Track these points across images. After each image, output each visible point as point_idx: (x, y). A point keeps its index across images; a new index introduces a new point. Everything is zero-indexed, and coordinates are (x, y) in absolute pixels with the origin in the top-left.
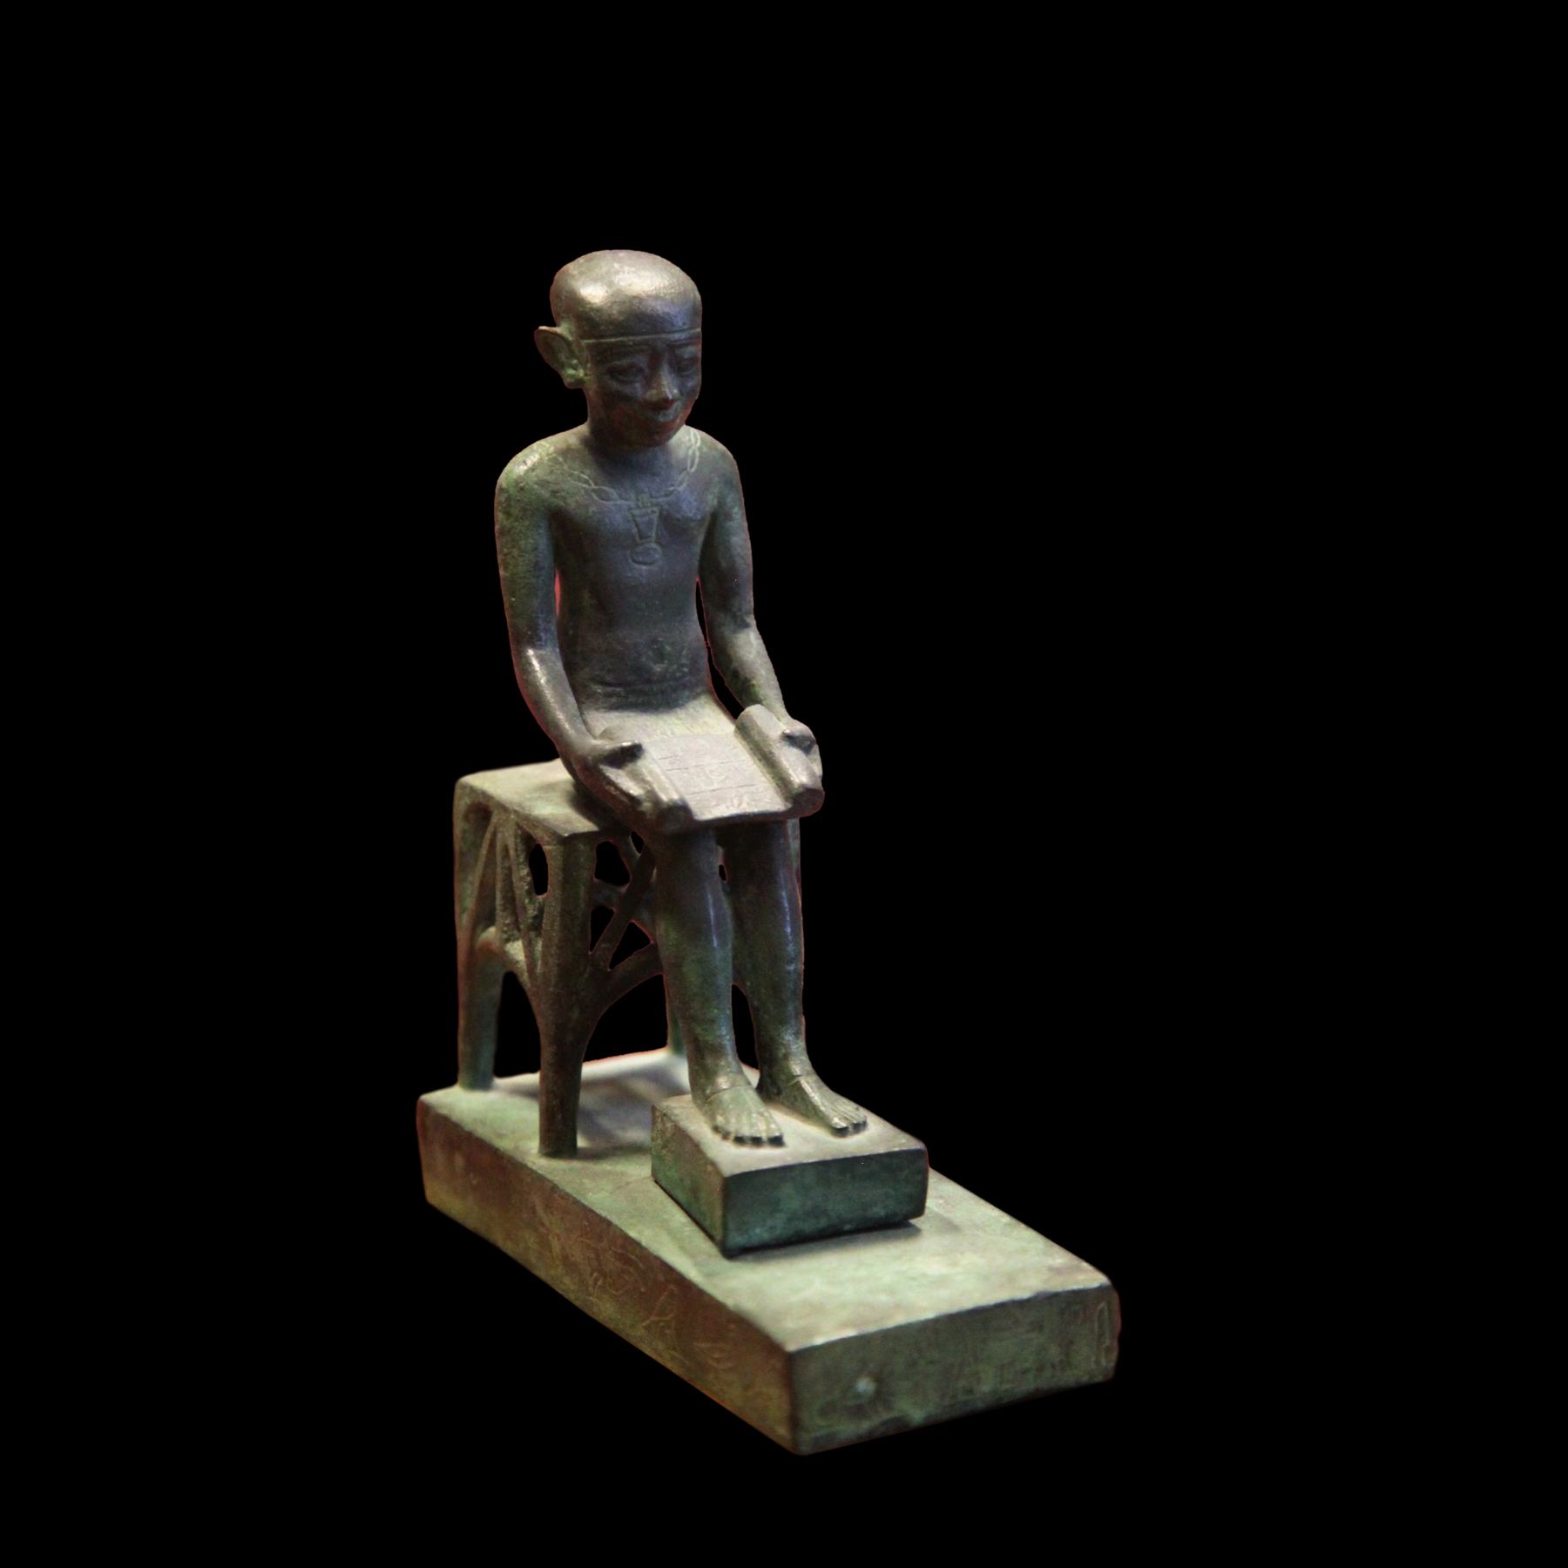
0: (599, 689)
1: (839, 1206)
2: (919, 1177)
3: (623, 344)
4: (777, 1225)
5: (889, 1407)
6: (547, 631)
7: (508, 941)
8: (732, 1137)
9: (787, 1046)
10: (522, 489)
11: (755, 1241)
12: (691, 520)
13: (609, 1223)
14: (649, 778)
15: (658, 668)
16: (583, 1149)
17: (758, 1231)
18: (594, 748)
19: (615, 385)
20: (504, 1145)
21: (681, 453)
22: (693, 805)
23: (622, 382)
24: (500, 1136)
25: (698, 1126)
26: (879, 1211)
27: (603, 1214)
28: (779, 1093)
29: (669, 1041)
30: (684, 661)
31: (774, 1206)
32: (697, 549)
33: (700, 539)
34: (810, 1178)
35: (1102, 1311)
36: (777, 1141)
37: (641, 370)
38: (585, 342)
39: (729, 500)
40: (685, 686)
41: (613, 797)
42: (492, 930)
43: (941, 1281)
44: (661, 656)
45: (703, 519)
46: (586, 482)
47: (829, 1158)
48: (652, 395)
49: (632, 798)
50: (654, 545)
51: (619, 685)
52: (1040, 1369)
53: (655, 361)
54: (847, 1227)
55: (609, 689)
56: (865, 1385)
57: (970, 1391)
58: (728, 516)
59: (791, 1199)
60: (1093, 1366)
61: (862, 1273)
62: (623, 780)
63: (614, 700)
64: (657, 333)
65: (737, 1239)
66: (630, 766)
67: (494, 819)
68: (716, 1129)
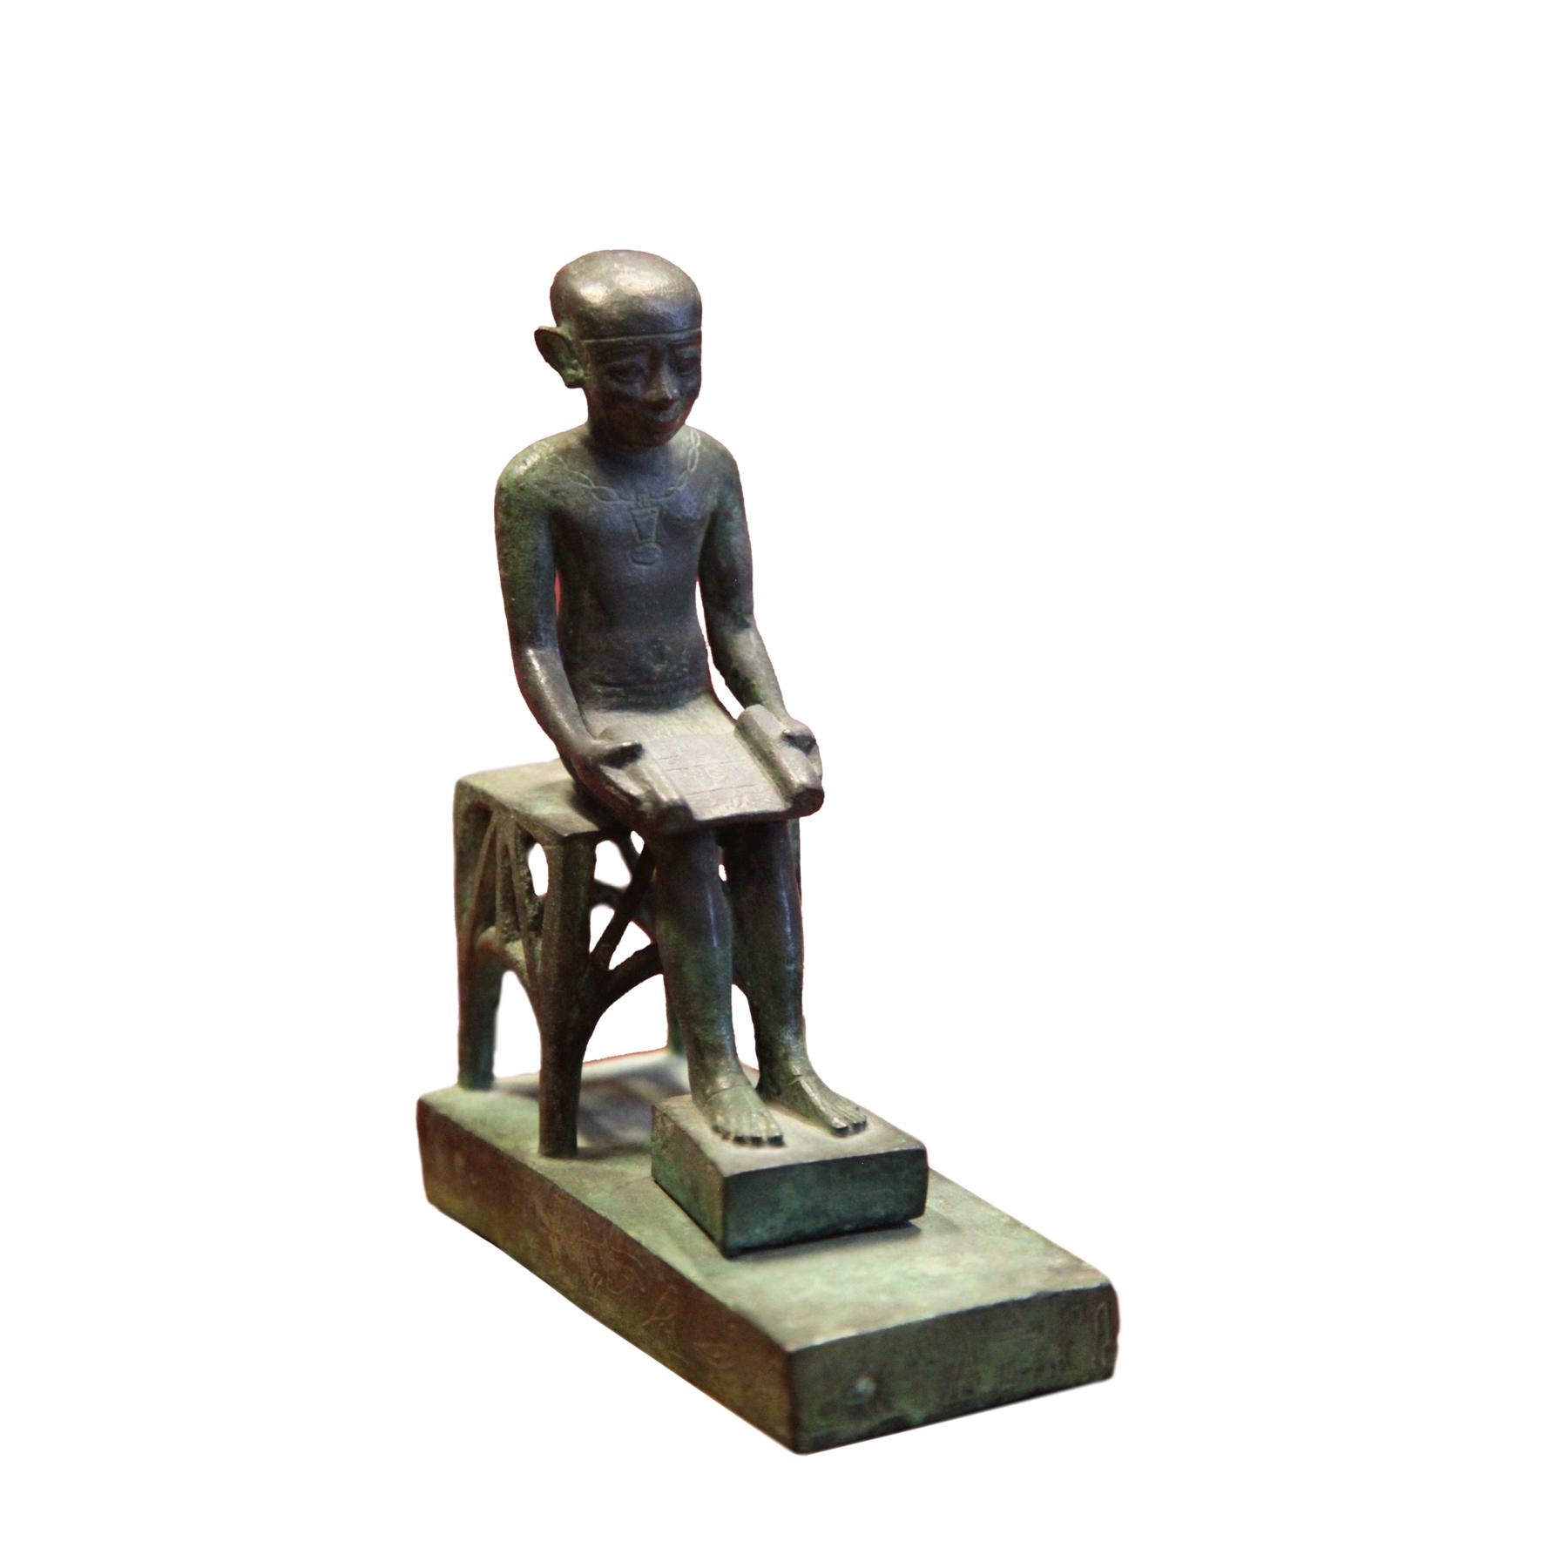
0: (599, 689)
1: (839, 1206)
3: (623, 344)
4: (777, 1225)
5: (889, 1407)
6: (547, 631)
7: (508, 941)
8: (732, 1137)
9: (787, 1046)
10: (522, 489)
11: (755, 1241)
12: (691, 520)
14: (649, 778)
15: (658, 668)
16: (583, 1149)
17: (758, 1231)
18: (594, 748)
19: (615, 385)
20: (504, 1145)
21: (681, 453)
22: (693, 805)
23: (622, 382)
24: (500, 1136)
25: (698, 1126)
26: (879, 1211)
27: (603, 1214)
28: (779, 1093)
30: (684, 661)
31: (774, 1206)
32: (697, 549)
33: (700, 539)
34: (810, 1178)
35: (1102, 1311)
36: (777, 1141)
37: (641, 370)
38: (585, 342)
39: (729, 500)
40: (685, 686)
41: (613, 797)
42: (492, 930)
43: (941, 1281)
44: (661, 656)
45: (703, 519)
46: (586, 482)
47: (829, 1158)
48: (652, 395)
49: (632, 798)
50: (654, 545)
51: (619, 685)
52: (1040, 1369)
53: (655, 361)
54: (847, 1227)
55: (609, 689)
56: (865, 1385)
57: (970, 1391)
59: (791, 1199)
60: (1093, 1366)
61: (862, 1273)
62: (623, 780)
63: (614, 700)
64: (657, 333)
65: (737, 1239)
66: (630, 766)
67: (494, 819)
68: (716, 1129)
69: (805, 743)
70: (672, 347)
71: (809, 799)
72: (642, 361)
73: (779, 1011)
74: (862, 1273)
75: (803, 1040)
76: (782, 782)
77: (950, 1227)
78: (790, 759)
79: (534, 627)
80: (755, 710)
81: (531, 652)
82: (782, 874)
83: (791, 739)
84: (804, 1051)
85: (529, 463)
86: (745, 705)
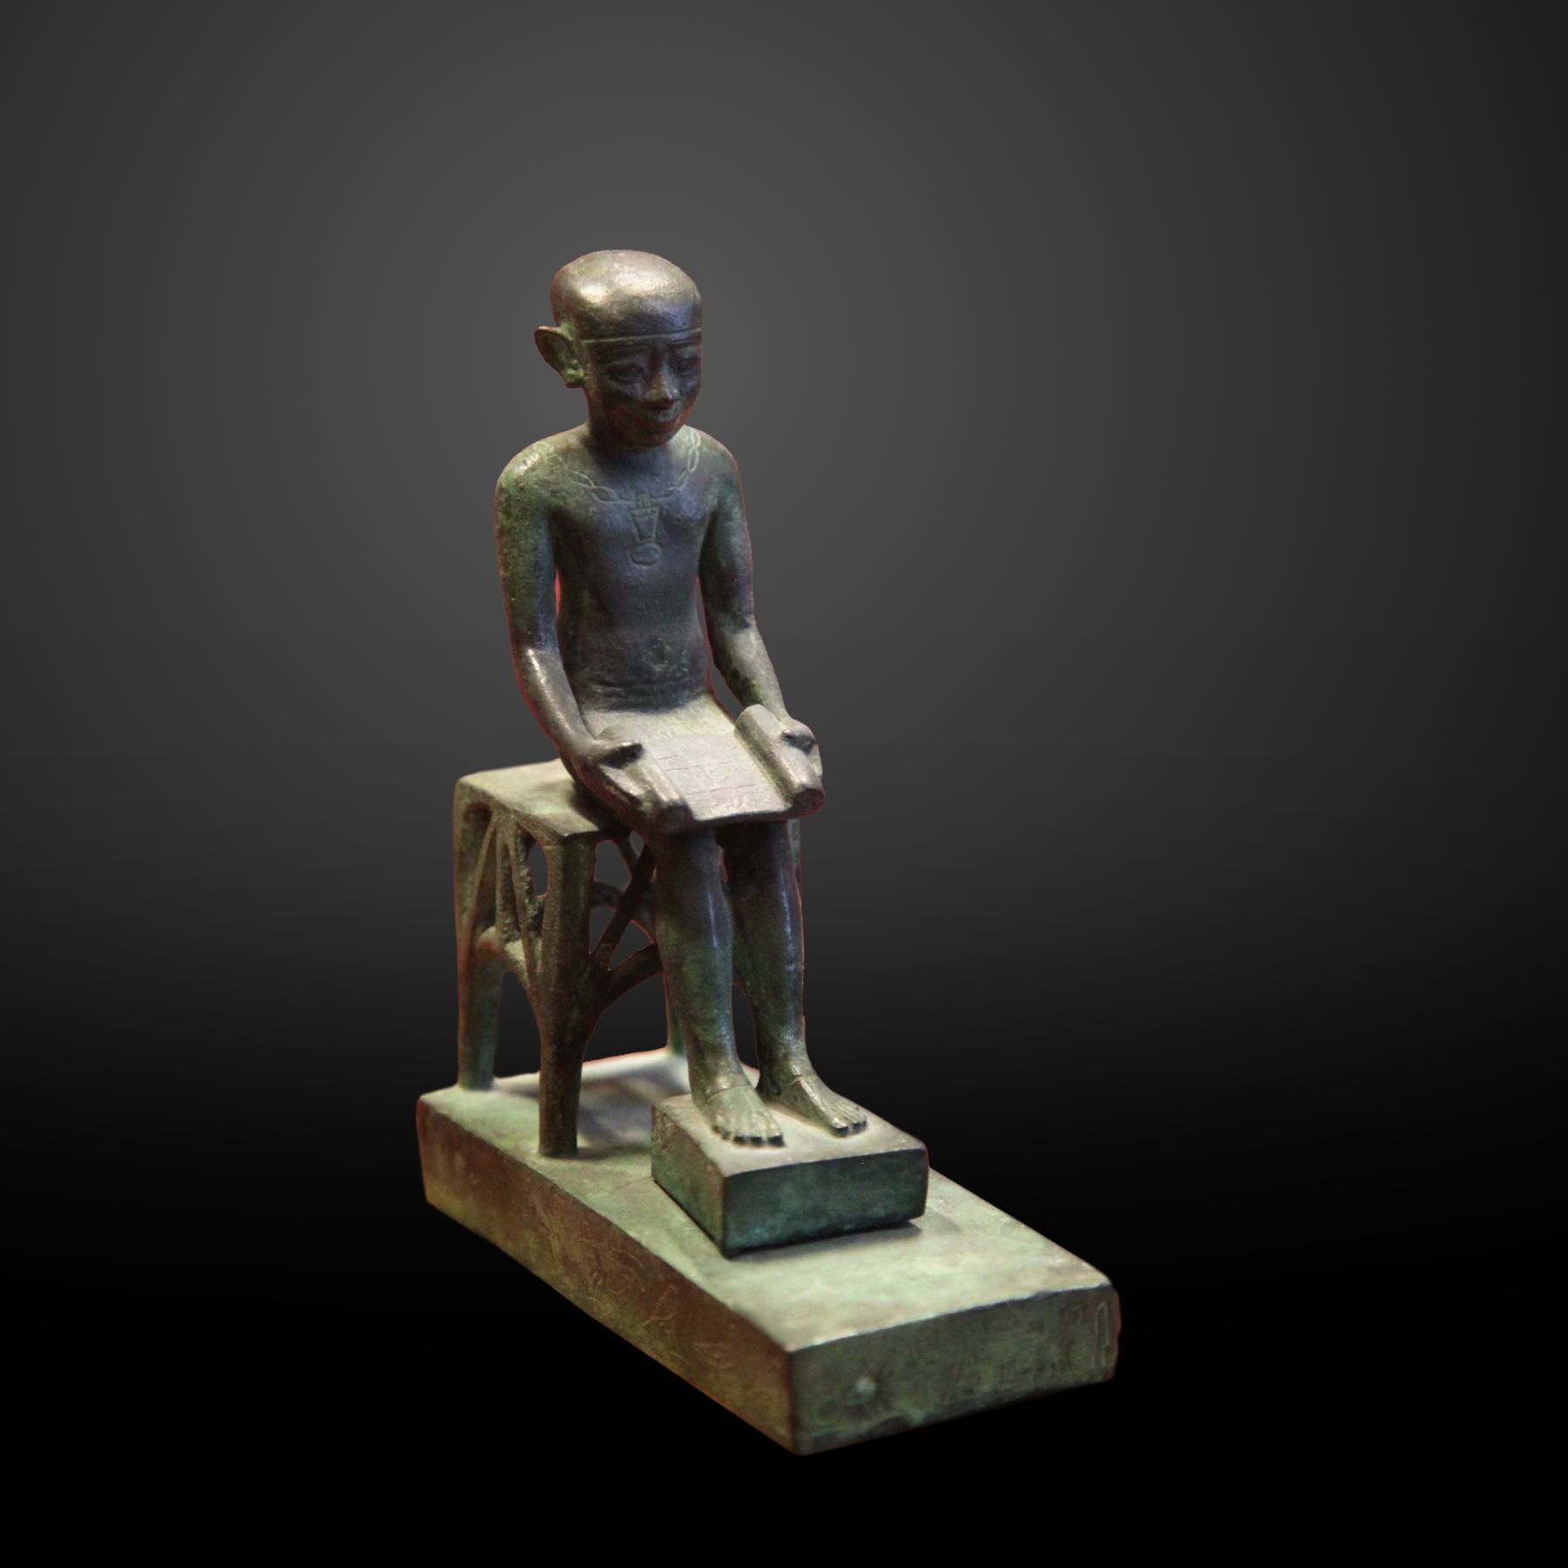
0: (599, 689)
1: (839, 1206)
2: (919, 1177)
3: (623, 344)
4: (777, 1225)
5: (889, 1407)
6: (547, 631)
7: (508, 941)
8: (732, 1137)
9: (787, 1046)
10: (522, 489)
11: (755, 1241)
12: (691, 520)
13: (609, 1223)
14: (649, 778)
15: (658, 668)
16: (583, 1149)
17: (758, 1231)
18: (594, 748)
19: (615, 385)
20: (504, 1145)
21: (681, 453)
22: (693, 805)
23: (622, 382)
24: (500, 1136)
25: (698, 1126)
26: (879, 1211)
27: (603, 1214)
28: (779, 1093)
29: (669, 1041)
30: (684, 661)
31: (774, 1206)
32: (697, 549)
33: (700, 539)
34: (810, 1178)
35: (1102, 1311)
36: (777, 1141)
37: (641, 370)
38: (585, 342)
39: (729, 500)
40: (685, 686)
41: (613, 797)
42: (492, 930)
43: (941, 1281)
44: (661, 656)
45: (703, 519)
46: (586, 482)
47: (829, 1158)
48: (652, 395)
49: (632, 798)
50: (654, 545)
51: (619, 685)
52: (1040, 1369)
53: (655, 361)
54: (847, 1227)
55: (609, 689)
56: (865, 1385)
57: (970, 1391)
58: (728, 516)
59: (791, 1199)
60: (1093, 1366)
61: (862, 1273)
62: (623, 780)
63: (614, 700)
64: (657, 333)
65: (737, 1239)
66: (630, 766)
67: (494, 819)
68: (716, 1129)
70: (672, 347)
72: (642, 361)
79: (534, 627)
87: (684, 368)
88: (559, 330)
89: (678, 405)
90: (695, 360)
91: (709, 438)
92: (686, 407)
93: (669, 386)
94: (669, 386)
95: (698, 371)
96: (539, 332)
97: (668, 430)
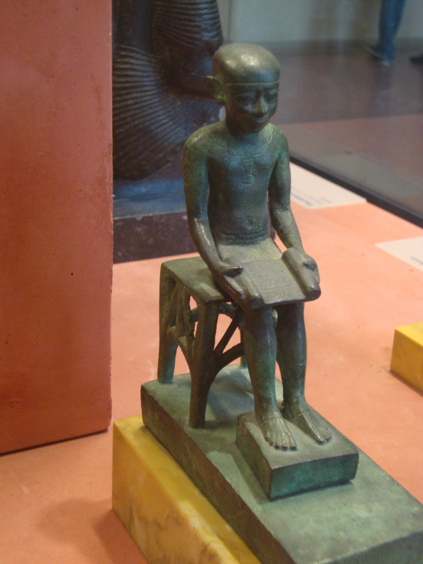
0: (224, 236)
4: (293, 486)
6: (203, 210)
7: (180, 336)
8: (274, 445)
9: (298, 398)
10: (195, 148)
11: (282, 493)
12: (267, 164)
13: (217, 471)
14: (245, 284)
15: (249, 228)
16: (209, 422)
17: (284, 490)
18: (222, 267)
20: (175, 416)
21: (265, 135)
22: (264, 297)
24: (174, 411)
25: (257, 433)
27: (216, 465)
28: (293, 417)
30: (261, 225)
32: (269, 177)
33: (270, 173)
36: (293, 449)
38: (228, 84)
39: (283, 156)
40: (260, 236)
41: (229, 290)
42: (174, 327)
43: (366, 523)
44: (251, 223)
45: (272, 164)
46: (224, 147)
47: (317, 458)
48: (256, 110)
49: (238, 293)
50: (251, 176)
51: (233, 235)
59: (299, 476)
61: (330, 515)
62: (233, 282)
63: (230, 241)
64: (260, 82)
65: (274, 493)
66: (238, 277)
67: (177, 285)
68: (267, 439)
69: (312, 266)
70: (266, 89)
71: (314, 294)
72: (252, 95)
73: (294, 378)
74: (330, 515)
75: (304, 394)
76: (303, 285)
77: (368, 483)
78: (306, 274)
79: (198, 208)
80: (291, 250)
81: (196, 220)
82: (299, 326)
83: (306, 265)
84: (304, 399)
85: (199, 137)
86: (287, 247)
87: (271, 98)
88: (216, 78)
89: (266, 116)
90: (276, 95)
91: (274, 126)
92: (270, 116)
93: (265, 106)
94: (265, 106)
95: (276, 100)
96: (399, 338)
97: (262, 126)
